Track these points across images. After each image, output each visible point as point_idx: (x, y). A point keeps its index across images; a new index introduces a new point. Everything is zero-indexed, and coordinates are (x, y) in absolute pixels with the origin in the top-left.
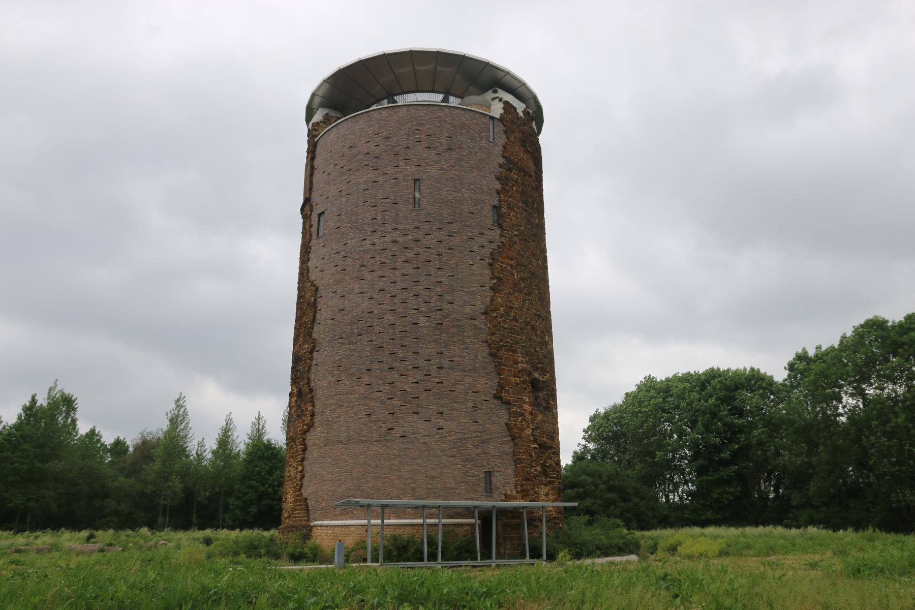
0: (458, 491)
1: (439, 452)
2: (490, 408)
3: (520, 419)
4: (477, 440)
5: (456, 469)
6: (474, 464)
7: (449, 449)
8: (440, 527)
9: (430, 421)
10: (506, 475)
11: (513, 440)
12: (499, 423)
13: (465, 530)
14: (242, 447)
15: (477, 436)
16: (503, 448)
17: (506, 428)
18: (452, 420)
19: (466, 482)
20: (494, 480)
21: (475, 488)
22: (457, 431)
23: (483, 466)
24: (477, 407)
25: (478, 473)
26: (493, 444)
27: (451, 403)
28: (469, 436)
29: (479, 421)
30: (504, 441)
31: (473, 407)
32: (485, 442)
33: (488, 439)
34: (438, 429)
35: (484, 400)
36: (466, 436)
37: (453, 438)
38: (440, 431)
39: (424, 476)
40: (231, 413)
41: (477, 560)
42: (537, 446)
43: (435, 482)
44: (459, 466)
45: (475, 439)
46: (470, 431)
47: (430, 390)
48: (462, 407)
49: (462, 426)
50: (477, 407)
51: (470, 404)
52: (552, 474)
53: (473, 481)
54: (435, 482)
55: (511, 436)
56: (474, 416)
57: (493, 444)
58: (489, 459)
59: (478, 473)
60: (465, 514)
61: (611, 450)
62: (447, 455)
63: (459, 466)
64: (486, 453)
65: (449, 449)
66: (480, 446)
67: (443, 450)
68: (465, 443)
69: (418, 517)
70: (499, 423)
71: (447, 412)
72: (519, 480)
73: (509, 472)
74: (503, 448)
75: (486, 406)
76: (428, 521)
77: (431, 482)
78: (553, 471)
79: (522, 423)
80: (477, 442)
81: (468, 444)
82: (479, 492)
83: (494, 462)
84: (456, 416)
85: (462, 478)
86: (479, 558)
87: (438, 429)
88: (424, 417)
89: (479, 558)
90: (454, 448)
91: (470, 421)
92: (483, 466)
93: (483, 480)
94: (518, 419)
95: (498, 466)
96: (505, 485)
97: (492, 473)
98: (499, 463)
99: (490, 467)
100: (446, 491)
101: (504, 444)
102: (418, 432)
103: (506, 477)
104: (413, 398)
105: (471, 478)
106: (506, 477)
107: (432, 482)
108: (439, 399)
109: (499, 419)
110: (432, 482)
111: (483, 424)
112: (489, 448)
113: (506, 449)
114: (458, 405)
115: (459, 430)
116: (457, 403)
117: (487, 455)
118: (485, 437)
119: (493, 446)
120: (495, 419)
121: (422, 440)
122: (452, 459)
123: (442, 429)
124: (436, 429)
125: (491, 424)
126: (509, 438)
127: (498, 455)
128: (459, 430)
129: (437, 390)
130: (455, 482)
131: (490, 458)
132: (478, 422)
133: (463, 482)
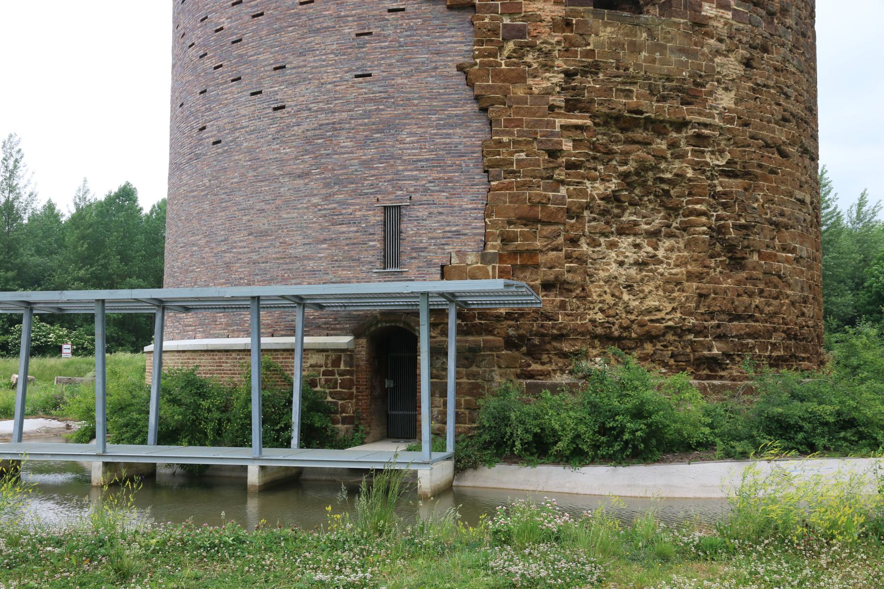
0: (311, 263)
1: (274, 169)
2: (410, 28)
3: (510, 46)
4: (365, 124)
5: (307, 208)
6: (354, 191)
7: (296, 158)
8: (254, 359)
9: (260, 92)
10: (451, 214)
11: (484, 110)
12: (436, 68)
13: (311, 366)
14: (146, 210)
15: (367, 114)
16: (448, 136)
17: (461, 79)
18: (304, 80)
19: (332, 241)
20: (408, 228)
21: (352, 253)
22: (314, 107)
23: (379, 192)
24: (370, 34)
25: (363, 212)
26: (415, 129)
27: (302, 37)
28: (345, 115)
29: (374, 73)
30: (449, 117)
31: (358, 35)
32: (390, 127)
33: (397, 116)
34: (275, 109)
35: (390, 11)
36: (337, 117)
37: (305, 126)
38: (278, 114)
39: (246, 233)
40: (880, 201)
41: (287, 444)
42: (589, 122)
43: (265, 244)
44: (315, 200)
45: (360, 121)
46: (348, 102)
47: (262, 14)
48: (328, 41)
49: (329, 91)
50: (370, 34)
51: (350, 30)
52: (688, 203)
53: (351, 235)
54: (265, 244)
55: (477, 98)
56: (358, 59)
57: (415, 129)
58: (397, 173)
59: (363, 212)
60: (326, 323)
61: (492, 19)
62: (290, 174)
63: (315, 200)
64: (392, 157)
65: (296, 158)
66: (374, 141)
67: (281, 162)
68: (332, 136)
69: (233, 331)
70: (436, 68)
71: (293, 61)
72: (494, 224)
73: (466, 202)
74: (448, 136)
75: (396, 27)
76: (267, 341)
77: (257, 246)
78: (690, 194)
79: (521, 57)
80: (364, 130)
81: (342, 139)
82: (363, 263)
83: (416, 179)
84: (313, 68)
85: (322, 229)
86: (295, 442)
87: (275, 109)
88: (250, 87)
89: (295, 442)
90: (307, 152)
91: (348, 76)
92: (379, 192)
93: (379, 231)
94: (501, 48)
95: (426, 190)
96: (443, 241)
97: (403, 211)
98: (430, 182)
99: (399, 193)
100: (285, 267)
101: (452, 126)
102: (239, 126)
103: (450, 218)
104: (234, 42)
105: (344, 228)
106: (450, 218)
107: (260, 245)
108: (277, 31)
109: (435, 58)
110: (260, 245)
111: (385, 79)
112: (402, 142)
113: (456, 140)
114: (318, 39)
115: (321, 105)
116: (317, 32)
117: (392, 162)
118: (388, 113)
119: (411, 134)
120: (423, 57)
121: (245, 144)
122: (301, 182)
123: (283, 107)
124: (270, 110)
125: (409, 75)
126: (472, 107)
127: (427, 160)
128: (321, 105)
129: (276, 9)
130: (306, 241)
131: (400, 168)
132: (370, 75)
133: (325, 241)
